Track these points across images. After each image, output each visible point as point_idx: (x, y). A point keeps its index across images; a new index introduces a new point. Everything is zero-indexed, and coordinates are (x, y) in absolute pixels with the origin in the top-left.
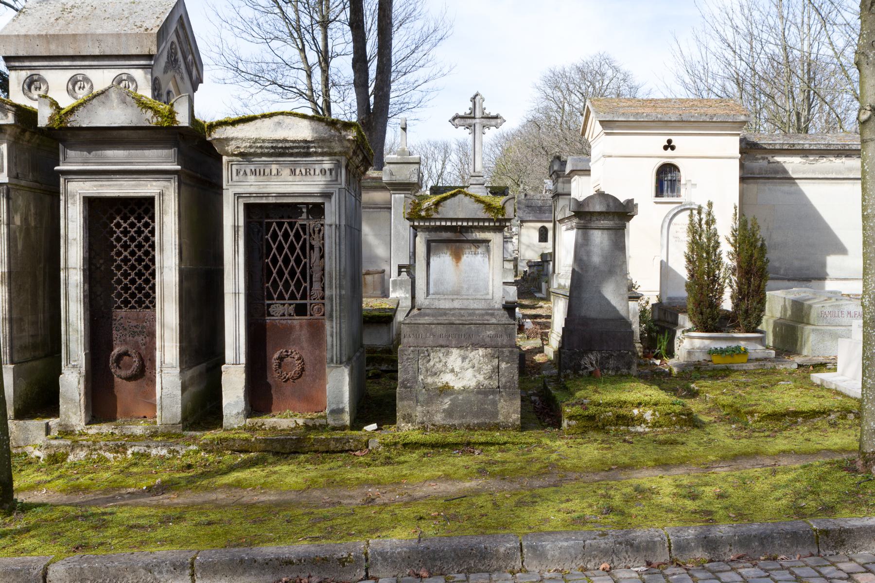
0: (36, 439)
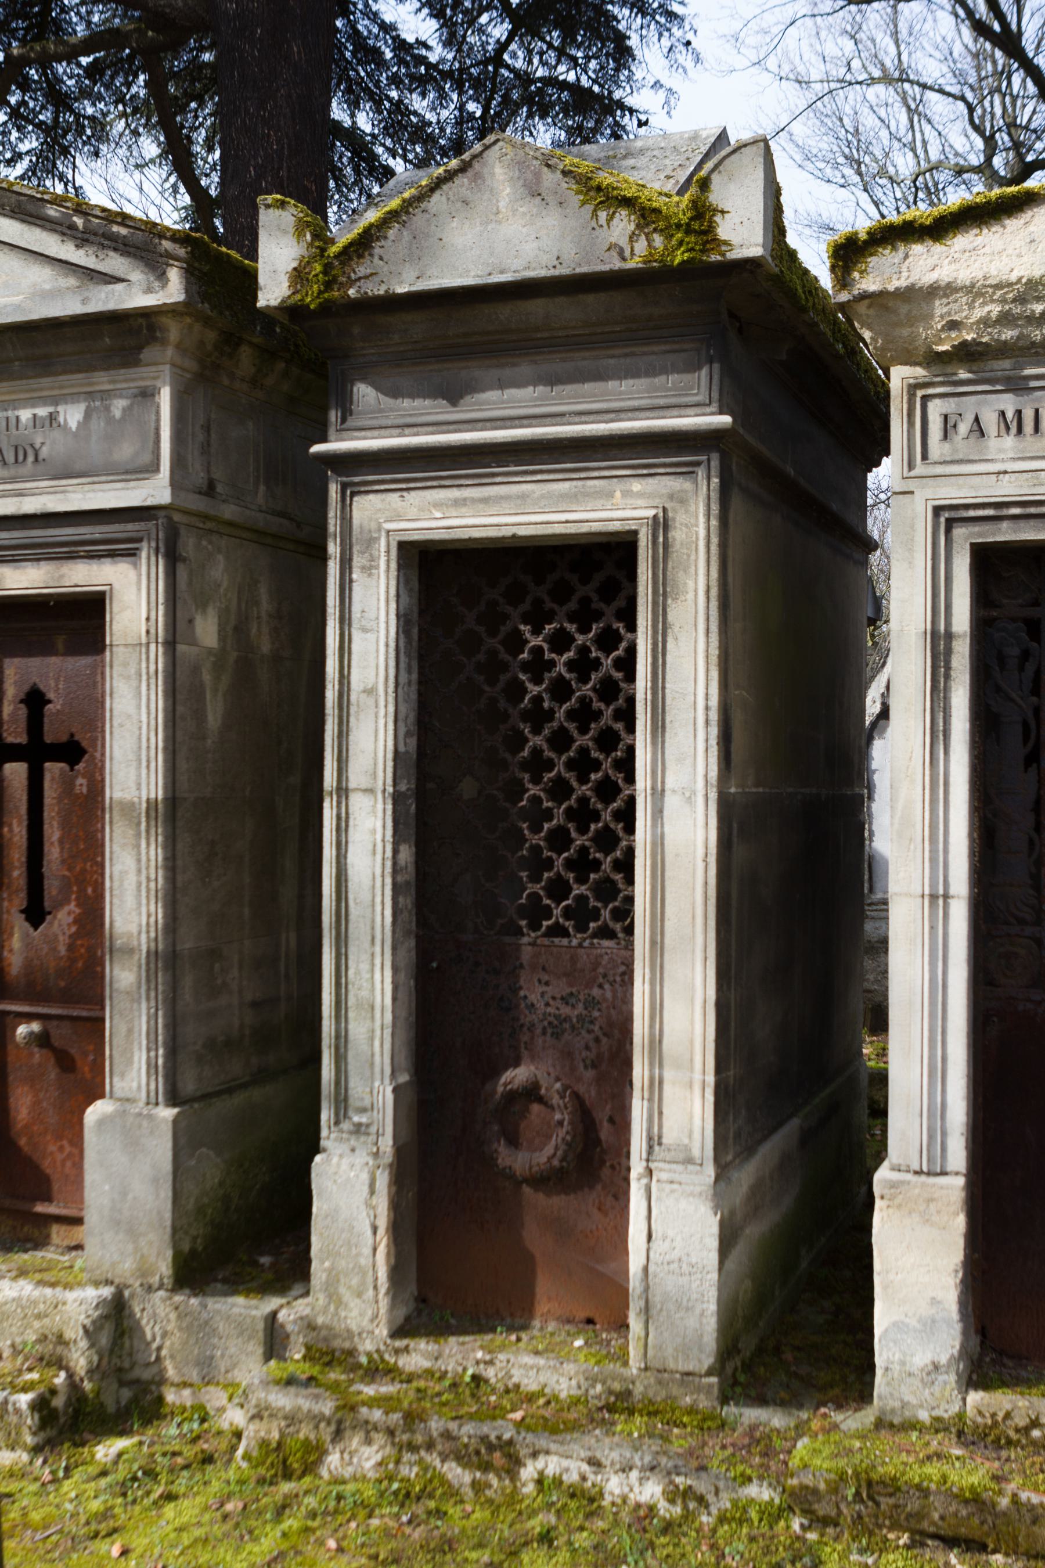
0: (234, 1366)
